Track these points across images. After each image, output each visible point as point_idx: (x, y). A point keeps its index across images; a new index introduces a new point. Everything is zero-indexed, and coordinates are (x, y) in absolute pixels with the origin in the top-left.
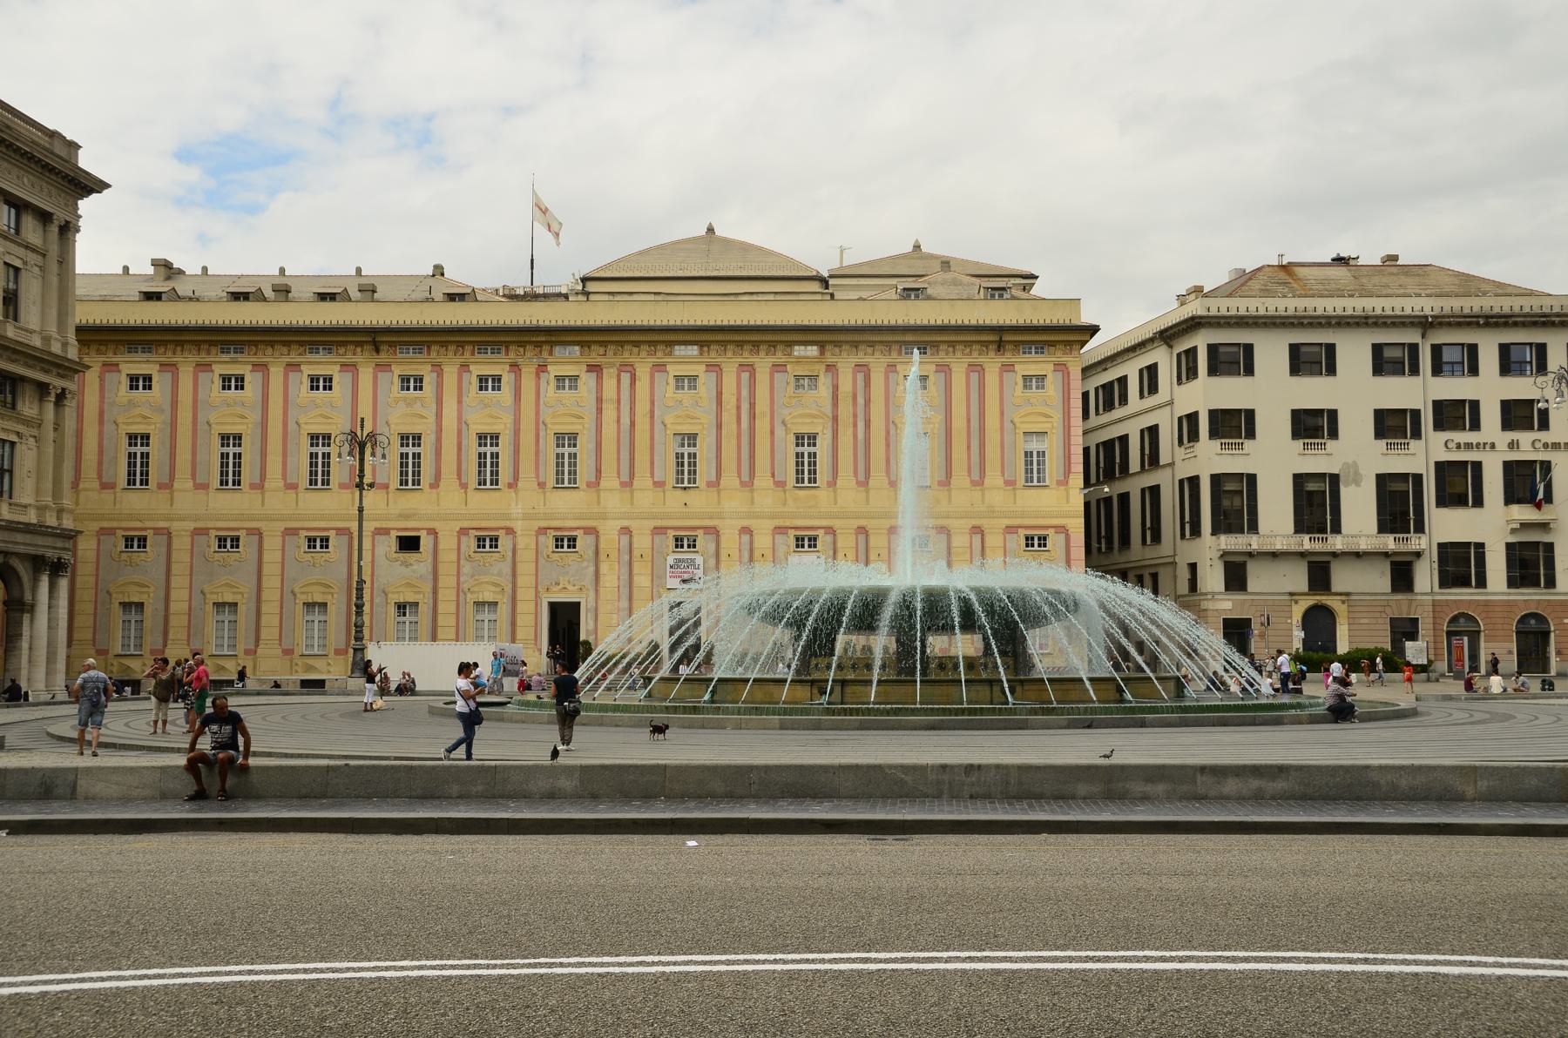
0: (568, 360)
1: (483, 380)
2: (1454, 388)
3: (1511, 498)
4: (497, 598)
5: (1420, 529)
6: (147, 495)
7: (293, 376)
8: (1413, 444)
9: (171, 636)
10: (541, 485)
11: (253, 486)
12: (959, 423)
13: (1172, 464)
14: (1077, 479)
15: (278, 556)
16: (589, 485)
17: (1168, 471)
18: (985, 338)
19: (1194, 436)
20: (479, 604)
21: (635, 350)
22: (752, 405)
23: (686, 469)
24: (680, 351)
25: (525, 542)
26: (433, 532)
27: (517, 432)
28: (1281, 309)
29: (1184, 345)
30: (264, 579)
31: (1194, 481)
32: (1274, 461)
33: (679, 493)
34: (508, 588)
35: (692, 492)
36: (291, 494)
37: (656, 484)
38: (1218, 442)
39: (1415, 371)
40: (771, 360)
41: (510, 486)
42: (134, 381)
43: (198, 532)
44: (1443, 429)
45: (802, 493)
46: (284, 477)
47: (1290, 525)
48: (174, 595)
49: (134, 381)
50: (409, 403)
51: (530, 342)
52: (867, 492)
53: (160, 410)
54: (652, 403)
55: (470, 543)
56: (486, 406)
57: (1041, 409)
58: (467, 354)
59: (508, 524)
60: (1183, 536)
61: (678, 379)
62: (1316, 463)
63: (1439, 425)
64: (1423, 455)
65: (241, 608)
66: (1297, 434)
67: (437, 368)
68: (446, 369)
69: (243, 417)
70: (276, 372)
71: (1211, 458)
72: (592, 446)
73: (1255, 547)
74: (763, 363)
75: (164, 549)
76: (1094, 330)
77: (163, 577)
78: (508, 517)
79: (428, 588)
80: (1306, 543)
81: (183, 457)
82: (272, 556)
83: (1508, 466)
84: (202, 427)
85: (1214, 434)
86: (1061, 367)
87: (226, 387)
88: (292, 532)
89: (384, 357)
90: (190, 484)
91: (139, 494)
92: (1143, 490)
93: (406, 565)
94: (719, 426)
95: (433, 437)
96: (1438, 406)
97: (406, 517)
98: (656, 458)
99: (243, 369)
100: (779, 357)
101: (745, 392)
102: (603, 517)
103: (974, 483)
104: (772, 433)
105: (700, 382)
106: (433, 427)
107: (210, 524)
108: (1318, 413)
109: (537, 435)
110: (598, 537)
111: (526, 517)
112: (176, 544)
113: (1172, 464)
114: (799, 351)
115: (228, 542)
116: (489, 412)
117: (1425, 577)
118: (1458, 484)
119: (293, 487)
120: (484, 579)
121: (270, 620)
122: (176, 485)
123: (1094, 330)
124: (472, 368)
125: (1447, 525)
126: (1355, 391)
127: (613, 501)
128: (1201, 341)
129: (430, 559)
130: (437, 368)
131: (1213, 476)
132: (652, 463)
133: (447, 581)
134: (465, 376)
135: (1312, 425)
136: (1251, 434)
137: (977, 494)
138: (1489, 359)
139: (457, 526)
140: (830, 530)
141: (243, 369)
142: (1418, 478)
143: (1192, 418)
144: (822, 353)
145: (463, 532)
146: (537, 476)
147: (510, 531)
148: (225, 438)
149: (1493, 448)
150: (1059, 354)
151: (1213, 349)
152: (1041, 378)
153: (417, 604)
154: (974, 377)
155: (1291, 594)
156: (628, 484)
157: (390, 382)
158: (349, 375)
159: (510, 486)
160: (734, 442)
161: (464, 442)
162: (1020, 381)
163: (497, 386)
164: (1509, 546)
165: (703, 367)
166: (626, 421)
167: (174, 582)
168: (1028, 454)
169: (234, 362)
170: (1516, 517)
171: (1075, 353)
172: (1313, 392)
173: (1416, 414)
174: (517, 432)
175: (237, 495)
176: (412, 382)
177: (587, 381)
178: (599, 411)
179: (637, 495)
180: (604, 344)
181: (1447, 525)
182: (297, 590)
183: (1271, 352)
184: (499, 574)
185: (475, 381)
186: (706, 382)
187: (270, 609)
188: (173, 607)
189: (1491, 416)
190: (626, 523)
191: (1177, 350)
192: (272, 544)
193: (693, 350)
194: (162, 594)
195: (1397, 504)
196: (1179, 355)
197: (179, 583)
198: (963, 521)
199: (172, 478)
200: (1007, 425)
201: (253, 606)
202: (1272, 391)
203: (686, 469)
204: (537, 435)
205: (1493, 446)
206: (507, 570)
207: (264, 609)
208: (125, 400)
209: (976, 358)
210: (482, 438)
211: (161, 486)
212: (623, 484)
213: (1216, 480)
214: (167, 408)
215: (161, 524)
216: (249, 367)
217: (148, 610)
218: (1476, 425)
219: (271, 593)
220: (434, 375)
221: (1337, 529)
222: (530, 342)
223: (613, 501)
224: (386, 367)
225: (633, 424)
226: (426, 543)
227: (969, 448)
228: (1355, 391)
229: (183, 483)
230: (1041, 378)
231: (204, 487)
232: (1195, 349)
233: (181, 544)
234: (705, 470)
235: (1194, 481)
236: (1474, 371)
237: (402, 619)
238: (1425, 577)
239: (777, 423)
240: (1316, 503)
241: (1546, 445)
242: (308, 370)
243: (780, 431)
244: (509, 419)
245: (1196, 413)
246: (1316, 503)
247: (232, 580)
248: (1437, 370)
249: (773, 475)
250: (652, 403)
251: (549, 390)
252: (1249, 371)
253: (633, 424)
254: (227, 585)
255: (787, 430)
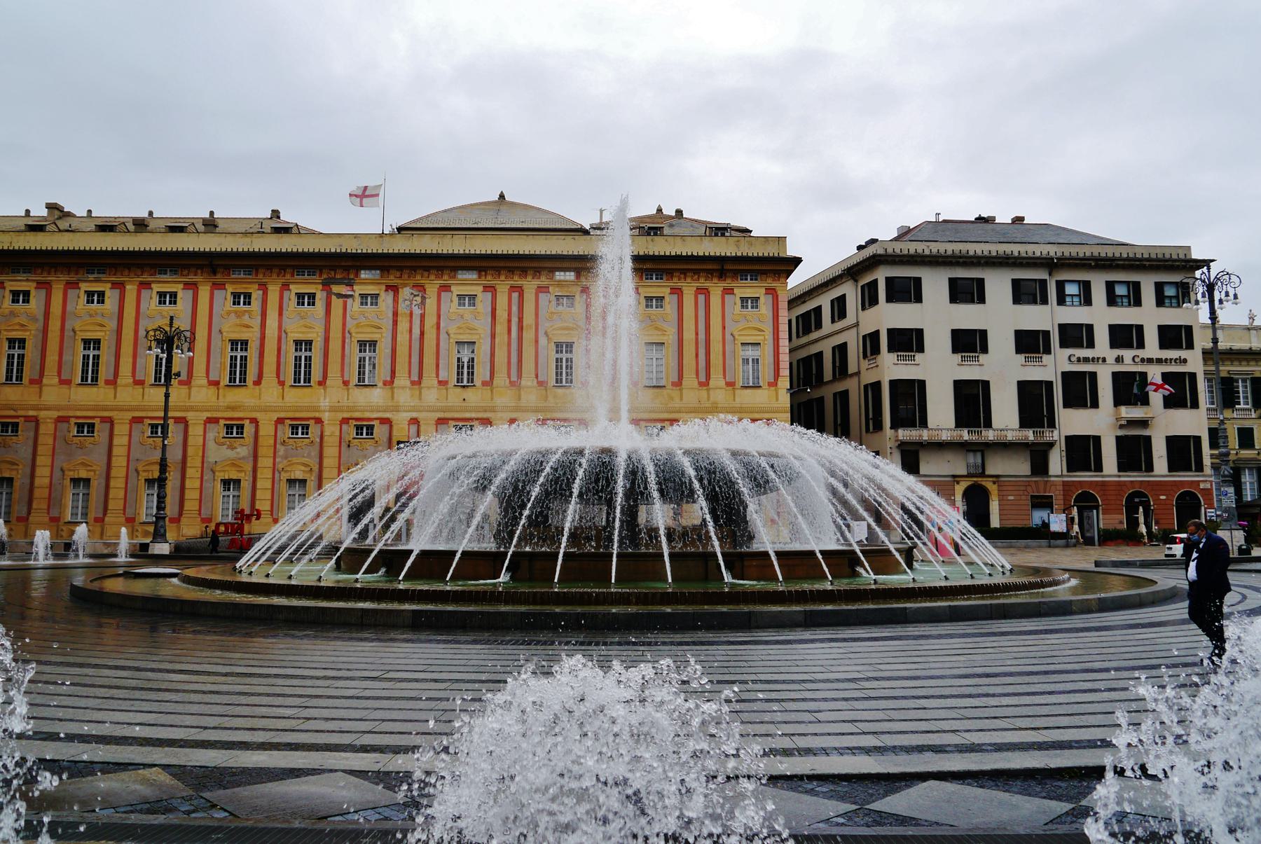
0: (467, 283)
1: (300, 296)
2: (1074, 314)
3: (1119, 401)
4: (306, 476)
5: (1052, 425)
6: (21, 388)
7: (145, 293)
8: (1045, 357)
9: (35, 506)
10: (346, 383)
11: (107, 382)
12: (689, 335)
13: (858, 374)
14: (784, 383)
15: (125, 440)
16: (385, 383)
17: (855, 379)
18: (710, 267)
19: (876, 350)
20: (291, 482)
21: (426, 274)
22: (521, 320)
23: (465, 374)
24: (462, 275)
25: (331, 430)
26: (254, 421)
27: (327, 340)
28: (1045, 253)
29: (867, 279)
30: (114, 459)
31: (877, 386)
32: (939, 370)
33: (459, 390)
34: (316, 468)
35: (469, 390)
36: (139, 389)
37: (440, 382)
38: (959, 356)
39: (1045, 301)
40: (536, 283)
41: (320, 383)
42: (15, 295)
43: (61, 419)
44: (1067, 347)
45: (560, 391)
46: (134, 375)
47: (951, 422)
48: (38, 472)
49: (15, 295)
50: (239, 315)
51: (518, 268)
52: (115, 389)
53: (35, 319)
54: (439, 317)
55: (217, 431)
56: (302, 318)
57: (750, 327)
58: (288, 276)
59: (317, 415)
60: (867, 430)
61: (461, 297)
62: (970, 373)
63: (1064, 344)
64: (1054, 366)
65: (94, 483)
66: (956, 349)
67: (263, 287)
68: (270, 288)
69: (248, 327)
70: (131, 289)
71: (891, 367)
72: (389, 351)
73: (925, 438)
74: (530, 285)
75: (32, 434)
76: (796, 261)
77: (30, 457)
78: (316, 409)
79: (249, 467)
80: (1030, 435)
81: (52, 358)
82: (120, 441)
83: (1116, 376)
84: (68, 333)
85: (891, 349)
86: (771, 291)
87: (90, 301)
88: (138, 420)
89: (219, 278)
90: (56, 380)
91: (15, 388)
92: (835, 395)
93: (232, 448)
94: (493, 336)
95: (258, 343)
96: (1063, 327)
97: (233, 409)
98: (441, 362)
99: (105, 287)
100: (543, 281)
101: (515, 309)
102: (396, 409)
103: (701, 384)
104: (537, 341)
105: (478, 300)
106: (258, 335)
107: (71, 413)
108: (972, 332)
109: (344, 342)
110: (391, 426)
111: (333, 409)
112: (42, 429)
113: (858, 374)
114: (559, 276)
115: (86, 427)
116: (305, 322)
117: (1057, 463)
118: (1080, 390)
119: (140, 383)
120: (295, 460)
121: (117, 492)
122: (45, 381)
123: (796, 261)
124: (291, 287)
125: (1073, 422)
126: (1000, 314)
127: (404, 396)
128: (881, 275)
129: (252, 440)
130: (263, 287)
131: (891, 382)
132: (438, 366)
133: (265, 462)
134: (286, 293)
135: (969, 342)
136: (921, 349)
137: (704, 393)
138: (1148, 294)
139: (275, 416)
140: (386, 421)
141: (29, 286)
142: (1049, 384)
143: (875, 336)
144: (578, 276)
145: (280, 421)
146: (342, 376)
147: (319, 421)
148: (87, 343)
149: (1106, 363)
150: (769, 280)
151: (889, 281)
152: (756, 300)
153: (239, 481)
154: (701, 298)
155: (954, 476)
156: (418, 383)
157: (223, 299)
158: (191, 292)
159: (320, 383)
160: (505, 348)
161: (283, 347)
162: (739, 302)
163: (312, 303)
164: (1117, 438)
165: (481, 288)
166: (416, 331)
167: (39, 461)
168: (746, 361)
169: (97, 281)
170: (1124, 415)
171: (782, 280)
172: (968, 316)
173: (1046, 334)
174: (327, 340)
175: (94, 389)
176: (241, 298)
177: (386, 299)
178: (395, 323)
179: (194, 390)
180: (400, 269)
181: (1073, 422)
182: (140, 468)
183: (935, 284)
184: (309, 456)
185: (294, 299)
186: (484, 300)
187: (117, 484)
188: (37, 482)
189: (1102, 337)
190: (415, 415)
191: (861, 283)
192: (121, 429)
193: (473, 276)
194: (28, 471)
195: (1034, 402)
196: (863, 287)
197: (43, 461)
198: (429, 414)
199: (42, 374)
200: (728, 337)
201: (103, 482)
202: (936, 314)
203: (465, 374)
204: (344, 342)
205: (1104, 360)
206: (314, 452)
207: (112, 484)
208: (7, 312)
209: (703, 283)
210: (298, 343)
211: (32, 382)
212: (413, 383)
213: (893, 383)
214: (41, 318)
215: (31, 413)
216: (109, 285)
217: (17, 484)
218: (1091, 345)
219: (119, 470)
220: (325, 294)
221: (988, 424)
222: (504, 268)
223: (404, 396)
224: (221, 286)
225: (422, 333)
226: (249, 429)
227: (697, 355)
228: (1000, 314)
229: (51, 379)
230: (756, 300)
231: (67, 382)
232: (875, 282)
233: (47, 429)
234: (481, 373)
235: (877, 386)
236: (1138, 303)
237: (227, 493)
238: (1057, 463)
239: (541, 332)
240: (973, 402)
241: (1143, 360)
242: (156, 288)
243: (543, 341)
244: (320, 329)
245: (877, 332)
246: (973, 402)
247: (89, 461)
248: (1061, 300)
249: (537, 376)
250: (439, 317)
251: (354, 306)
252: (982, 300)
253: (422, 333)
254: (83, 464)
255: (549, 339)
